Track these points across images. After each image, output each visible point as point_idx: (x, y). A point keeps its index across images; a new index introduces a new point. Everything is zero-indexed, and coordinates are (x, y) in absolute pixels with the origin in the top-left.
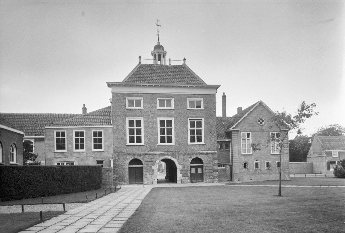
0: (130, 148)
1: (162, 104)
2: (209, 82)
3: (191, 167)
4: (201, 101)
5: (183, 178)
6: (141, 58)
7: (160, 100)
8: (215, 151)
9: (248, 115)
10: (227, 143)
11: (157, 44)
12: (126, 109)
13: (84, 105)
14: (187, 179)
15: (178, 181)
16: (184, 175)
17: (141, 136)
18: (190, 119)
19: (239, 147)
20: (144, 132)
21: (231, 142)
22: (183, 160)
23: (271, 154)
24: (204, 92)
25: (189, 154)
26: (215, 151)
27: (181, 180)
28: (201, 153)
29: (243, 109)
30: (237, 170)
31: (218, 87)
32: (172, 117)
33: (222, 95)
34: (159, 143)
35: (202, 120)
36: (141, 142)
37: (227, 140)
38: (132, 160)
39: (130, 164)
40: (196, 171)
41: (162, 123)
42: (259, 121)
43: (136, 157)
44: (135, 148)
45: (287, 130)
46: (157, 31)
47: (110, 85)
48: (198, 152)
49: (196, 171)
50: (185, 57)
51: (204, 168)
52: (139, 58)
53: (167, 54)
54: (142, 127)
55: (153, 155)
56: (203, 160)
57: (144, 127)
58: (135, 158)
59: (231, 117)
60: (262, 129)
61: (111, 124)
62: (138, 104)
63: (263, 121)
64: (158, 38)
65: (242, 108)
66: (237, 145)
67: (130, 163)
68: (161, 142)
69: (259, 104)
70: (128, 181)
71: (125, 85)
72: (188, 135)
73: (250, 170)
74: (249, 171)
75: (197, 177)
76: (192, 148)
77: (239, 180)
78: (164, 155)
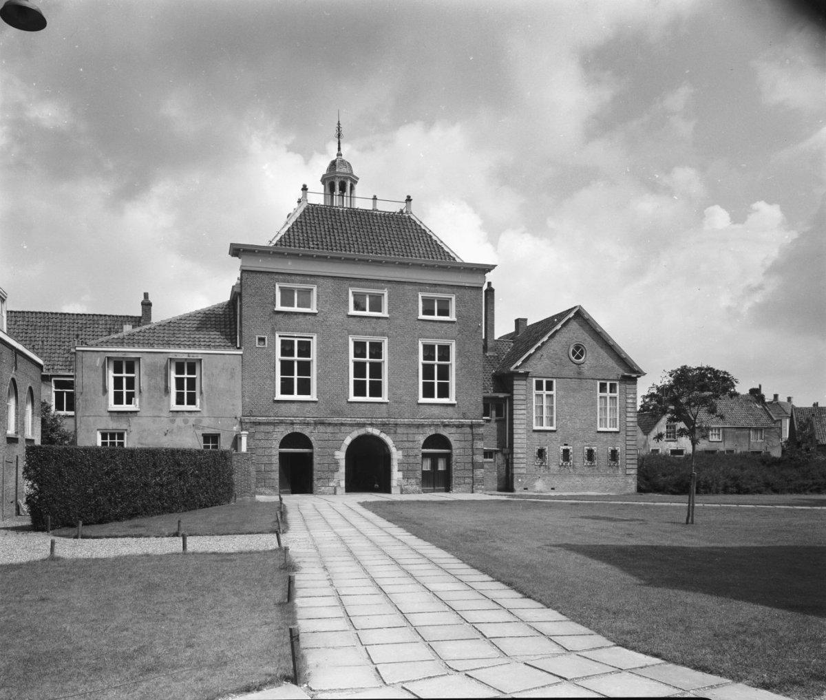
0: (283, 406)
4: (448, 301)
5: (404, 482)
6: (306, 189)
7: (282, 289)
13: (146, 295)
14: (414, 485)
18: (281, 335)
19: (528, 413)
21: (511, 399)
22: (406, 439)
27: (401, 486)
29: (529, 323)
30: (522, 465)
31: (489, 271)
32: (383, 334)
35: (312, 338)
37: (501, 395)
38: (289, 435)
39: (282, 445)
40: (434, 465)
41: (360, 348)
42: (574, 353)
43: (298, 429)
44: (294, 407)
45: (635, 376)
47: (237, 251)
49: (434, 465)
50: (306, 183)
51: (454, 458)
52: (303, 189)
53: (359, 181)
56: (451, 439)
57: (318, 356)
60: (579, 373)
61: (238, 346)
63: (582, 353)
65: (526, 320)
66: (523, 407)
72: (275, 371)
73: (552, 467)
74: (548, 468)
75: (439, 479)
76: (428, 410)
77: (525, 489)
78: (363, 425)
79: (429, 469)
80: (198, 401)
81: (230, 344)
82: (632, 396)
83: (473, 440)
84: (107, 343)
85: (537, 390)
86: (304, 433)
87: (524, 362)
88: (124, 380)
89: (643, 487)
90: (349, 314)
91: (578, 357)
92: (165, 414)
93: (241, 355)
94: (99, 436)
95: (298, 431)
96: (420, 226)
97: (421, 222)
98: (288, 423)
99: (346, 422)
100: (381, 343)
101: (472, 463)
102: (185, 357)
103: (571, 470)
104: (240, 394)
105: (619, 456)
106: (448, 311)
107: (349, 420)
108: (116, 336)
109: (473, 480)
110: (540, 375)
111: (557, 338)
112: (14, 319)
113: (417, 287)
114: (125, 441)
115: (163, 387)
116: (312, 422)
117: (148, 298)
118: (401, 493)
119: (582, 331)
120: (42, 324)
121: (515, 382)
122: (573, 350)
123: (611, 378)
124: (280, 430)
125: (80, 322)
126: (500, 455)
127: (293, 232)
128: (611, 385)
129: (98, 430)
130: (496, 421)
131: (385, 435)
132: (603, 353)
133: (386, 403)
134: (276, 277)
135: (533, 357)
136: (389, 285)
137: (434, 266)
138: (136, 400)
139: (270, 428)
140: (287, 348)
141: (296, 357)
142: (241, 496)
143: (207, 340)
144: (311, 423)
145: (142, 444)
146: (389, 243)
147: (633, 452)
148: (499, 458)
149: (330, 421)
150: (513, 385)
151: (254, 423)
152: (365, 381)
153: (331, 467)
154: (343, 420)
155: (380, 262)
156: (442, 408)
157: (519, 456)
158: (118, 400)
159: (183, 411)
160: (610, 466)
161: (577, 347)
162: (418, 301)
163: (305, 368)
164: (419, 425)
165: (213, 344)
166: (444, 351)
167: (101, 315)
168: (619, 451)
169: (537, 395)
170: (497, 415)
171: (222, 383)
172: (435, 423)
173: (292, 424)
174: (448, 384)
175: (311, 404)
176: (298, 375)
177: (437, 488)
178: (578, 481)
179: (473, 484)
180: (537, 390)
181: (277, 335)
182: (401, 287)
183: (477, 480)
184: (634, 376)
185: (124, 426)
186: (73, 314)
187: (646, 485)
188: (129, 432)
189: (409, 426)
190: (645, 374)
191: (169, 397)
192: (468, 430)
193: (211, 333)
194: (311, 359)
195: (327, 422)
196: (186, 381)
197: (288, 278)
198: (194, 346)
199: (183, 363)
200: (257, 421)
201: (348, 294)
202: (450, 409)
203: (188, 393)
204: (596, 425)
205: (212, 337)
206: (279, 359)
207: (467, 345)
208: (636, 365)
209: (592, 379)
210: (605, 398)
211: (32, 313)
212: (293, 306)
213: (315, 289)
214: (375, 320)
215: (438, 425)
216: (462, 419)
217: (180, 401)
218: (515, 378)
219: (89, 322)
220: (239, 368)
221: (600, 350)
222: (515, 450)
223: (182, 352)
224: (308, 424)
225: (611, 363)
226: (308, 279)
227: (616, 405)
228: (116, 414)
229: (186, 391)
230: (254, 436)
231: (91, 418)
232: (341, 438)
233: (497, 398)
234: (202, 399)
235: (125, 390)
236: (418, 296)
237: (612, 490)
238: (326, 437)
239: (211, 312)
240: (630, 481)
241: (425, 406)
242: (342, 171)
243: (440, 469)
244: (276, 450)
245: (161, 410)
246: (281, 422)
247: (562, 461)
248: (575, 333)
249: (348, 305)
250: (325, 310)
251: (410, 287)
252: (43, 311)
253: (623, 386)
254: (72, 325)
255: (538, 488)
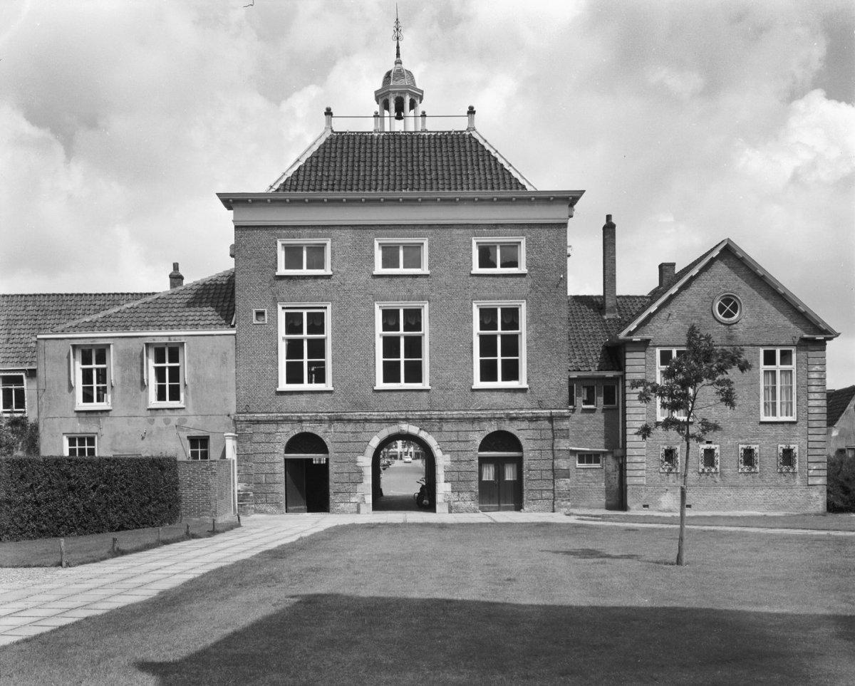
0: (288, 399)
1: (390, 261)
2: (539, 180)
3: (483, 461)
5: (454, 497)
6: (331, 114)
7: (385, 248)
8: (562, 411)
9: (681, 289)
10: (608, 384)
11: (391, 66)
12: (277, 276)
15: (437, 506)
16: (458, 485)
17: (481, 356)
20: (333, 349)
23: (762, 420)
24: (516, 217)
25: (473, 420)
26: (562, 411)
27: (449, 502)
28: (515, 415)
30: (640, 473)
32: (422, 298)
33: (604, 222)
34: (380, 384)
35: (326, 308)
36: (419, 380)
37: (610, 374)
40: (499, 474)
41: (390, 318)
42: (721, 309)
43: (308, 428)
44: (304, 398)
46: (395, 24)
47: (230, 201)
48: (506, 412)
49: (499, 474)
50: (328, 106)
51: (525, 464)
52: (326, 114)
54: (328, 334)
55: (358, 421)
56: (521, 438)
58: (304, 431)
59: (642, 297)
61: (233, 324)
62: (317, 256)
63: (735, 308)
64: (398, 47)
65: (673, 265)
67: (290, 447)
68: (385, 381)
69: (721, 251)
70: (283, 503)
71: (273, 201)
72: (472, 358)
76: (486, 398)
77: (644, 506)
78: (396, 421)
79: (491, 479)
80: (182, 395)
81: (224, 322)
82: (818, 368)
83: (554, 438)
84: (77, 328)
85: (765, 364)
86: (316, 433)
87: (640, 326)
88: (95, 373)
89: (839, 503)
90: (375, 273)
91: (729, 315)
92: (143, 412)
93: (235, 335)
94: (66, 442)
95: (309, 430)
96: (483, 146)
97: (486, 141)
98: (294, 421)
99: (371, 417)
100: (420, 310)
101: (553, 470)
102: (166, 340)
103: (718, 480)
104: (234, 386)
105: (797, 459)
106: (517, 263)
107: (375, 415)
108: (88, 320)
109: (554, 494)
110: (667, 343)
111: (695, 287)
112: (23, 304)
113: (469, 231)
114: (96, 447)
115: (139, 379)
116: (326, 418)
117: (178, 269)
118: (450, 512)
119: (734, 276)
120: (54, 308)
121: (628, 355)
122: (720, 305)
123: (783, 343)
124: (286, 430)
125: (98, 303)
126: (610, 458)
127: (305, 171)
128: (783, 353)
129: (64, 434)
130: (604, 410)
131: (426, 433)
132: (768, 306)
133: (428, 391)
134: (278, 231)
135: (656, 317)
136: (431, 231)
137: (492, 200)
138: (108, 397)
139: (272, 428)
140: (293, 324)
141: (305, 335)
142: (199, 516)
143: (197, 318)
144: (325, 420)
145: (115, 450)
146: (434, 173)
147: (819, 452)
148: (610, 463)
149: (350, 417)
150: (625, 359)
151: (250, 421)
152: (399, 362)
153: (352, 478)
154: (367, 415)
155: (416, 200)
156: (507, 395)
157: (635, 459)
158: (88, 398)
159: (163, 409)
160: (781, 472)
161: (727, 300)
162: (471, 250)
163: (317, 348)
164: (474, 418)
165: (202, 323)
166: (511, 317)
167: (123, 294)
168: (796, 451)
169: (766, 372)
170: (605, 403)
171: (211, 372)
172: (497, 416)
173: (300, 421)
174: (517, 360)
175: (325, 395)
176: (308, 358)
177: (503, 505)
178: (728, 494)
179: (554, 499)
180: (765, 364)
181: (280, 307)
182: (446, 232)
183: (559, 493)
184: (820, 338)
185: (94, 429)
186: (91, 295)
187: (843, 499)
188: (100, 435)
189: (460, 420)
190: (838, 335)
191: (147, 392)
192: (546, 424)
193: (205, 309)
194: (422, 332)
195: (345, 417)
196: (167, 370)
197: (294, 232)
198: (178, 326)
199: (163, 349)
200: (255, 418)
201: (373, 246)
202: (521, 395)
203: (171, 387)
204: (759, 413)
205: (204, 314)
206: (283, 338)
207: (543, 306)
208: (823, 322)
209: (752, 345)
210: (774, 372)
211: (44, 295)
212: (301, 267)
213: (329, 243)
214: (410, 279)
215: (501, 418)
216: (537, 409)
217: (161, 396)
218: (627, 349)
219: (108, 303)
220: (232, 353)
221: (764, 302)
222: (629, 452)
223: (161, 335)
224: (321, 421)
225: (783, 321)
226: (320, 231)
227: (791, 383)
228: (84, 415)
229: (167, 384)
230: (252, 437)
231: (55, 420)
232: (366, 439)
233: (604, 378)
234: (186, 394)
235: (95, 385)
236: (471, 243)
237: (784, 507)
238: (345, 437)
239: (213, 283)
240: (815, 494)
241: (483, 393)
242: (399, 83)
243: (507, 479)
244: (280, 457)
245: (137, 408)
246: (286, 420)
247: (702, 466)
248: (724, 279)
249: (373, 262)
250: (343, 270)
251: (461, 232)
252: (57, 292)
253: (803, 354)
254: (87, 307)
255: (665, 506)
